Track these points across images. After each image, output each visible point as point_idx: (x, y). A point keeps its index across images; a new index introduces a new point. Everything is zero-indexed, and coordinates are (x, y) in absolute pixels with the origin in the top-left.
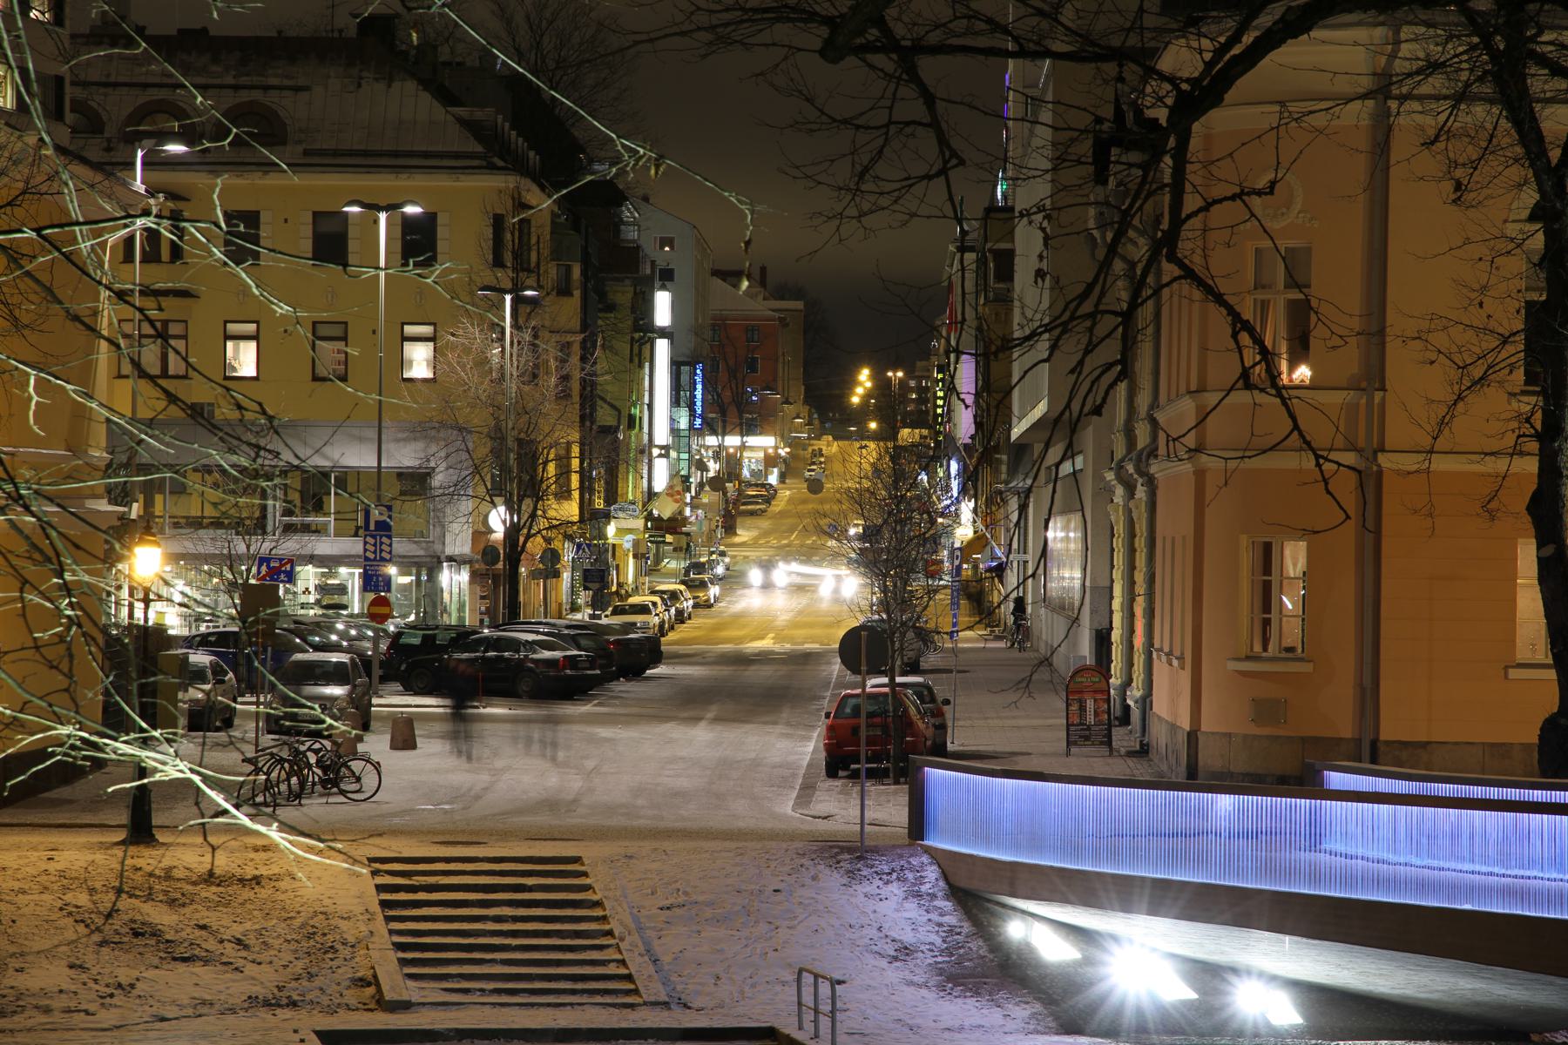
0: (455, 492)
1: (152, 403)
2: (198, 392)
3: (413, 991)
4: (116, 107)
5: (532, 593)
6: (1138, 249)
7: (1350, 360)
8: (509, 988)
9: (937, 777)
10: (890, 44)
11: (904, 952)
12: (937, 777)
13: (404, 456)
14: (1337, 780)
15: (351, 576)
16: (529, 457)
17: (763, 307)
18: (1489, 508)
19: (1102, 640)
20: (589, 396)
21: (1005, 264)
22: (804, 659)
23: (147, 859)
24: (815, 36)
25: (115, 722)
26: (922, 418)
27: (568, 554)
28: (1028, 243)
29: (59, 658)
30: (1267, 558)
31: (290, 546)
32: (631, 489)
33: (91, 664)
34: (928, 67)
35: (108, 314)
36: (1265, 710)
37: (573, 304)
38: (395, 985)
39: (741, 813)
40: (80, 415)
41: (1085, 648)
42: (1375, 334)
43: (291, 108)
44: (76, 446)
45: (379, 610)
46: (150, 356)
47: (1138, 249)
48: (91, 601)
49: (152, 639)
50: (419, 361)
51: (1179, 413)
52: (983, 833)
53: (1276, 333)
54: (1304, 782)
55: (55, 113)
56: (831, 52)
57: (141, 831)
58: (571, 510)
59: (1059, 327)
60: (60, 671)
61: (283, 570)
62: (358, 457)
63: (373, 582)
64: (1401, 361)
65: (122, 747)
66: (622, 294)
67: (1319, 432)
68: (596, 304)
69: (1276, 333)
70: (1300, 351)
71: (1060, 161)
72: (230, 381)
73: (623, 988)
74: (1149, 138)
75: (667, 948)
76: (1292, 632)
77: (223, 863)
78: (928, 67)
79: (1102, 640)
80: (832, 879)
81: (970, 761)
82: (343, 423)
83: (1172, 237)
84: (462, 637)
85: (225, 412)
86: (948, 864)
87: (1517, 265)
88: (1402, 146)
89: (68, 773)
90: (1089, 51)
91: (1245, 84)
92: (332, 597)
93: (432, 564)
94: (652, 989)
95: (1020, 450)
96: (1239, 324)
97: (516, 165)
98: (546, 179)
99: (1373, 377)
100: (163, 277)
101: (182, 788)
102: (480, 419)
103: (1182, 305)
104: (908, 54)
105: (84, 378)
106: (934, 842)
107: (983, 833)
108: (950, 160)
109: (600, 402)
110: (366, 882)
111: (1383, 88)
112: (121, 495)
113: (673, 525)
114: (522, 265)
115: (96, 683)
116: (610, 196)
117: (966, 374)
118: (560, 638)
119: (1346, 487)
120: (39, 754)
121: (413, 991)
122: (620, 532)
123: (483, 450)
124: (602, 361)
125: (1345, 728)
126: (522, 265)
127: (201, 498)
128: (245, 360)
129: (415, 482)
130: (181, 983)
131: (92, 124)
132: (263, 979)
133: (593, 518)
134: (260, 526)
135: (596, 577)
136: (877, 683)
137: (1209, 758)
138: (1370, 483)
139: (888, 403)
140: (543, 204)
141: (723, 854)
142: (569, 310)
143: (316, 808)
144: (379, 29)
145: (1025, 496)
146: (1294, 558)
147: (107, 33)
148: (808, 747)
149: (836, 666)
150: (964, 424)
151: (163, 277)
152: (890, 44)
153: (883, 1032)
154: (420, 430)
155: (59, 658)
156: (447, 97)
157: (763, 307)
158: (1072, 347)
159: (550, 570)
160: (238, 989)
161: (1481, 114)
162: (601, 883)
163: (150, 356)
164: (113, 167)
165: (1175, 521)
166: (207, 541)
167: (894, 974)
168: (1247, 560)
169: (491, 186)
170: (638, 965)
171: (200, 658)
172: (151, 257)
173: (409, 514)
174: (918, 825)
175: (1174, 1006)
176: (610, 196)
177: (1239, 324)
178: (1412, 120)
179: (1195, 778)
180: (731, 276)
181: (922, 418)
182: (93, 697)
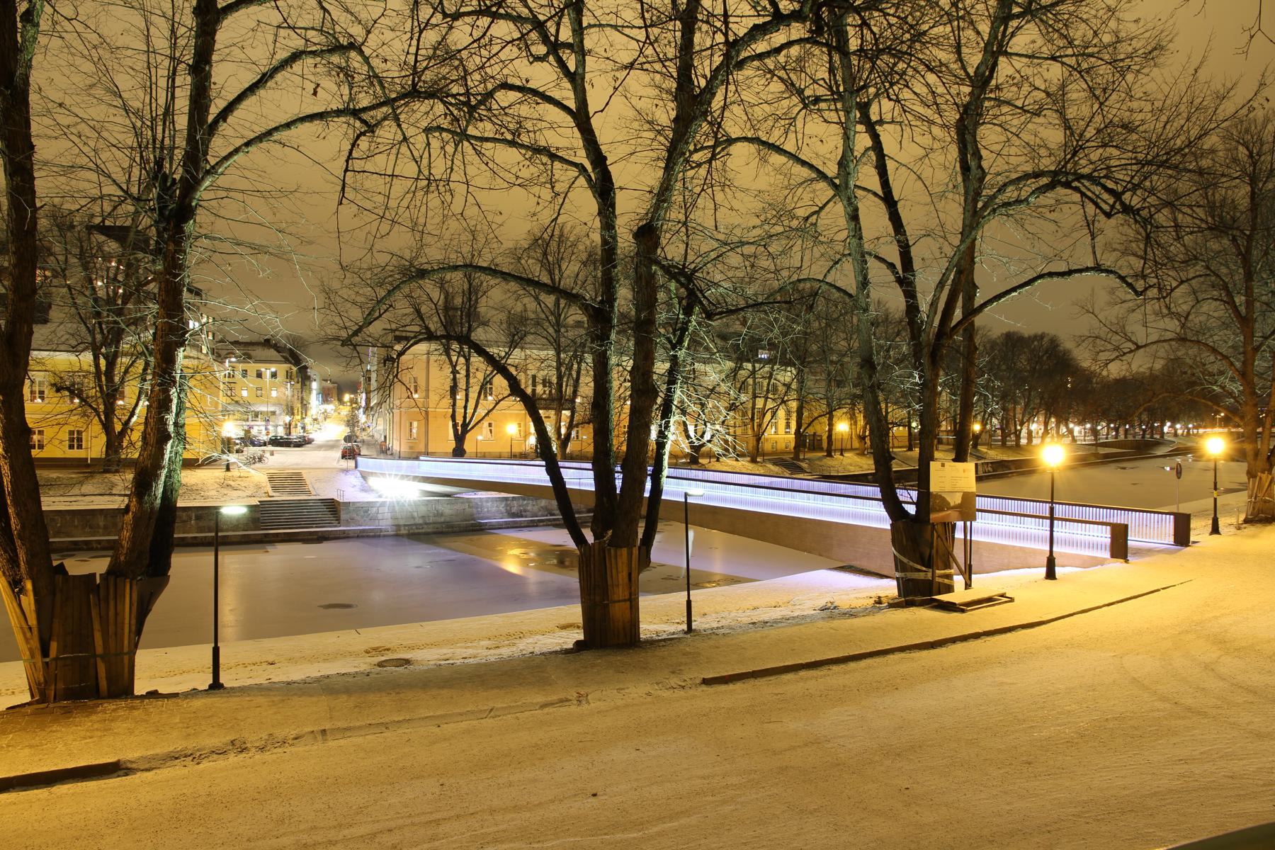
1: (229, 400)
2: (236, 399)
3: (274, 494)
4: (223, 353)
5: (293, 430)
6: (391, 377)
8: (290, 493)
9: (359, 459)
10: (352, 344)
12: (359, 459)
13: (272, 409)
14: (421, 458)
15: (263, 428)
16: (292, 409)
17: (331, 385)
18: (445, 417)
19: (385, 437)
21: (370, 379)
22: (338, 441)
23: (229, 474)
24: (340, 343)
25: (223, 452)
26: (356, 403)
27: (299, 424)
28: (374, 376)
29: (213, 443)
34: (358, 348)
35: (222, 386)
36: (411, 448)
37: (300, 385)
38: (271, 493)
39: (328, 465)
40: (217, 403)
41: (383, 439)
42: (427, 390)
43: (251, 353)
44: (216, 408)
46: (229, 393)
47: (391, 377)
49: (229, 440)
51: (397, 402)
53: (412, 389)
54: (417, 458)
55: (213, 354)
56: (343, 345)
57: (228, 469)
58: (299, 417)
59: (379, 389)
60: (1176, 288)
61: (251, 427)
66: (308, 383)
67: (420, 405)
68: (303, 384)
69: (412, 389)
70: (416, 391)
71: (379, 363)
72: (242, 397)
73: (309, 493)
74: (393, 360)
75: (316, 486)
76: (415, 435)
78: (358, 348)
79: (385, 437)
80: (343, 475)
82: (262, 403)
83: (397, 375)
84: (282, 438)
86: (361, 472)
87: (449, 380)
89: (215, 461)
90: (384, 346)
91: (408, 352)
92: (260, 432)
93: (277, 426)
94: (313, 493)
96: (408, 389)
97: (290, 363)
99: (427, 397)
100: (231, 380)
101: (234, 463)
102: (284, 403)
103: (398, 386)
104: (355, 346)
105: (218, 397)
106: (359, 469)
108: (362, 362)
111: (428, 353)
112: (224, 415)
113: (315, 420)
114: (291, 378)
115: (220, 447)
116: (306, 368)
117: (364, 395)
119: (423, 413)
120: (210, 458)
121: (274, 494)
122: (308, 421)
124: (304, 394)
126: (291, 378)
127: (238, 416)
129: (274, 413)
131: (219, 356)
132: (249, 493)
135: (303, 428)
136: (349, 444)
138: (427, 413)
140: (295, 369)
143: (258, 465)
144: (267, 341)
145: (373, 415)
146: (415, 424)
147: (222, 341)
148: (339, 454)
149: (343, 442)
150: (363, 404)
151: (231, 380)
152: (352, 344)
153: (286, 241)
154: (274, 405)
156: (279, 352)
157: (331, 385)
158: (381, 392)
159: (296, 427)
160: (244, 494)
161: (444, 357)
162: (305, 476)
163: (229, 393)
164: (222, 362)
165: (397, 419)
167: (353, 489)
168: (408, 425)
169: (286, 366)
171: (238, 441)
173: (273, 418)
174: (356, 467)
175: (410, 505)
176: (306, 368)
177: (408, 389)
178: (433, 358)
179: (400, 458)
180: (326, 380)
181: (356, 403)
182: (220, 449)
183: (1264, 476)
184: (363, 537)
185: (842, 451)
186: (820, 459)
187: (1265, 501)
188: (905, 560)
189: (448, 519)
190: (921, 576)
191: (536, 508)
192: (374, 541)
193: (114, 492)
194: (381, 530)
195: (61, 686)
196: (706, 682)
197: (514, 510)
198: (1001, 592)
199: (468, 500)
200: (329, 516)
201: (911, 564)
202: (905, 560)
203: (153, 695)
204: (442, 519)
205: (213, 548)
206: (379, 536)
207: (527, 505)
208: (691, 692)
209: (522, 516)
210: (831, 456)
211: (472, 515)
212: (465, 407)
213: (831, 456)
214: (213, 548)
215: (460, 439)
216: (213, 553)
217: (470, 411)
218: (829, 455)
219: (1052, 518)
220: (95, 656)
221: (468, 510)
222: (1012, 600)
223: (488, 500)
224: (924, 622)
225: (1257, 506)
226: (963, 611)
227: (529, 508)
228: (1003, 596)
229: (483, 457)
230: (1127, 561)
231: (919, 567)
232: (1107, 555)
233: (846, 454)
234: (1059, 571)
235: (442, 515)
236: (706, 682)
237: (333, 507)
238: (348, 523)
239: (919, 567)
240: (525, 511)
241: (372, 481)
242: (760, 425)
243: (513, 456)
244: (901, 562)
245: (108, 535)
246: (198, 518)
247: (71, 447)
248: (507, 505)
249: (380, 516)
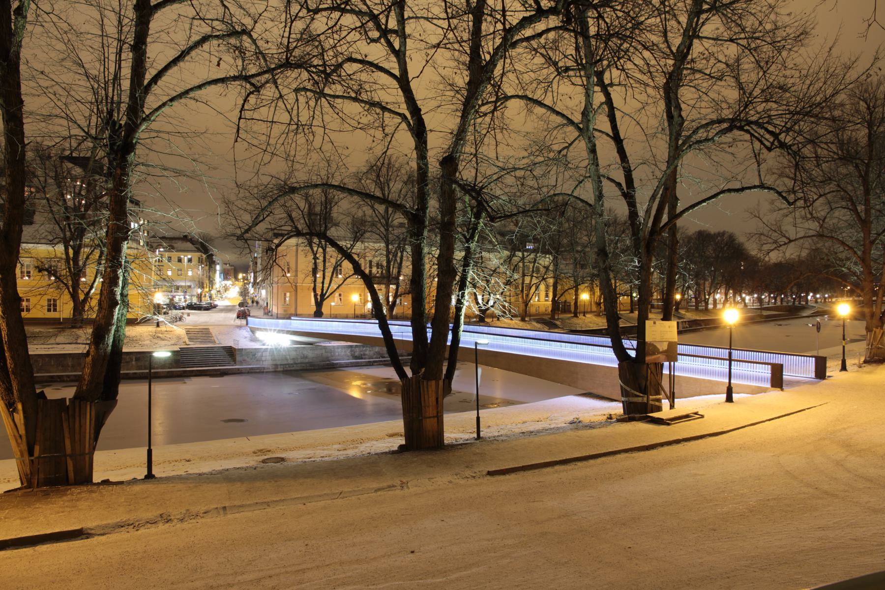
0: (194, 288)
1: (159, 278)
2: (164, 277)
4: (155, 245)
5: (203, 299)
6: (271, 262)
7: (294, 274)
8: (201, 342)
9: (249, 318)
10: (244, 239)
11: (246, 338)
12: (249, 318)
13: (188, 284)
15: (182, 297)
16: (203, 284)
17: (229, 267)
18: (309, 289)
19: (267, 303)
20: (210, 277)
21: (256, 263)
22: (234, 306)
23: (159, 329)
24: (236, 238)
25: (155, 314)
26: (247, 280)
28: (259, 261)
29: (148, 307)
30: (285, 294)
31: (175, 294)
32: (214, 287)
33: (152, 308)
34: (248, 242)
35: (154, 268)
36: (285, 311)
38: (188, 342)
39: (227, 323)
40: (150, 279)
41: (265, 304)
42: (296, 271)
43: (175, 245)
44: (150, 283)
45: (185, 301)
46: (159, 273)
47: (271, 262)
48: (152, 301)
49: (159, 305)
50: (190, 273)
51: (276, 279)
52: (254, 325)
53: (286, 270)
54: (289, 318)
55: (147, 245)
56: (237, 240)
57: (158, 325)
58: (207, 290)
59: (263, 270)
61: (174, 297)
62: (183, 284)
63: (185, 298)
64: (299, 274)
65: (156, 317)
66: (213, 266)
67: (291, 281)
68: (210, 267)
69: (286, 270)
71: (263, 252)
72: (168, 276)
73: (214, 342)
74: (272, 250)
75: (219, 337)
77: (168, 329)
78: (248, 242)
79: (267, 303)
80: (237, 330)
81: (253, 317)
82: (181, 280)
83: (275, 261)
85: (167, 279)
86: (251, 328)
88: (299, 251)
89: (149, 320)
90: (266, 240)
91: (283, 244)
92: (180, 300)
95: (258, 283)
96: (283, 270)
97: (201, 252)
98: (205, 253)
99: (296, 275)
100: (160, 264)
101: (163, 322)
102: (197, 280)
103: (276, 268)
105: (151, 275)
107: (254, 325)
108: (251, 252)
109: (596, 134)
110: (184, 331)
111: (297, 245)
112: (155, 288)
113: (219, 291)
115: (152, 310)
116: (212, 255)
117: (252, 275)
118: (207, 304)
119: (294, 287)
120: (145, 318)
122: (213, 292)
123: (197, 283)
125: (294, 313)
126: (202, 263)
127: (165, 288)
128: (169, 273)
129: (190, 287)
130: (163, 343)
132: (173, 342)
133: (210, 290)
134: (171, 292)
135: (211, 297)
136: (242, 308)
137: (279, 316)
138: (296, 287)
139: (244, 278)
140: (204, 256)
141: (756, 134)
142: (207, 268)
143: (178, 323)
146: (288, 295)
147: (154, 237)
148: (235, 315)
150: (252, 280)
151: (160, 264)
152: (244, 239)
154: (190, 281)
155: (148, 307)
156: (193, 244)
157: (229, 267)
158: (264, 272)
160: (170, 343)
161: (308, 248)
162: (211, 331)
163: (159, 273)
164: (154, 252)
165: (275, 291)
166: (166, 293)
168: (283, 295)
169: (199, 254)
170: (216, 340)
171: (165, 306)
172: (159, 261)
173: (189, 290)
174: (247, 324)
176: (212, 255)
177: (283, 270)
178: (300, 249)
179: (277, 318)
180: (226, 264)
183: (878, 330)
184: (252, 373)
185: (584, 313)
186: (569, 319)
187: (879, 348)
188: (628, 389)
189: (311, 361)
190: (639, 400)
191: (372, 353)
192: (259, 375)
193: (79, 342)
194: (264, 368)
195: (42, 476)
196: (490, 473)
197: (357, 354)
198: (695, 411)
199: (325, 348)
200: (228, 358)
201: (633, 391)
202: (628, 389)
203: (106, 482)
204: (307, 361)
205: (148, 381)
206: (263, 372)
207: (366, 350)
208: (480, 480)
209: (362, 358)
210: (577, 317)
211: (328, 357)
212: (323, 283)
213: (577, 317)
214: (148, 381)
215: (319, 304)
216: (148, 384)
217: (326, 285)
218: (576, 316)
219: (730, 360)
220: (65, 455)
221: (325, 354)
222: (702, 416)
223: (338, 347)
224: (642, 431)
225: (873, 351)
226: (669, 424)
227: (367, 353)
228: (696, 414)
229: (335, 317)
230: (782, 390)
231: (638, 394)
232: (769, 385)
233: (587, 316)
234: (735, 396)
235: (306, 357)
236: (490, 473)
237: (231, 352)
238: (241, 363)
239: (638, 394)
240: (365, 355)
241: (259, 335)
242: (527, 295)
243: (356, 317)
244: (626, 390)
245: (75, 371)
246: (137, 360)
247: (49, 310)
248: (351, 351)
249: (263, 359)
